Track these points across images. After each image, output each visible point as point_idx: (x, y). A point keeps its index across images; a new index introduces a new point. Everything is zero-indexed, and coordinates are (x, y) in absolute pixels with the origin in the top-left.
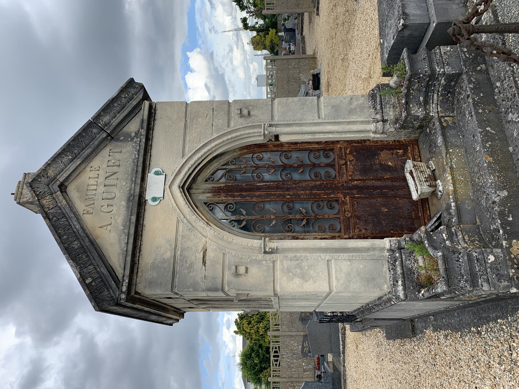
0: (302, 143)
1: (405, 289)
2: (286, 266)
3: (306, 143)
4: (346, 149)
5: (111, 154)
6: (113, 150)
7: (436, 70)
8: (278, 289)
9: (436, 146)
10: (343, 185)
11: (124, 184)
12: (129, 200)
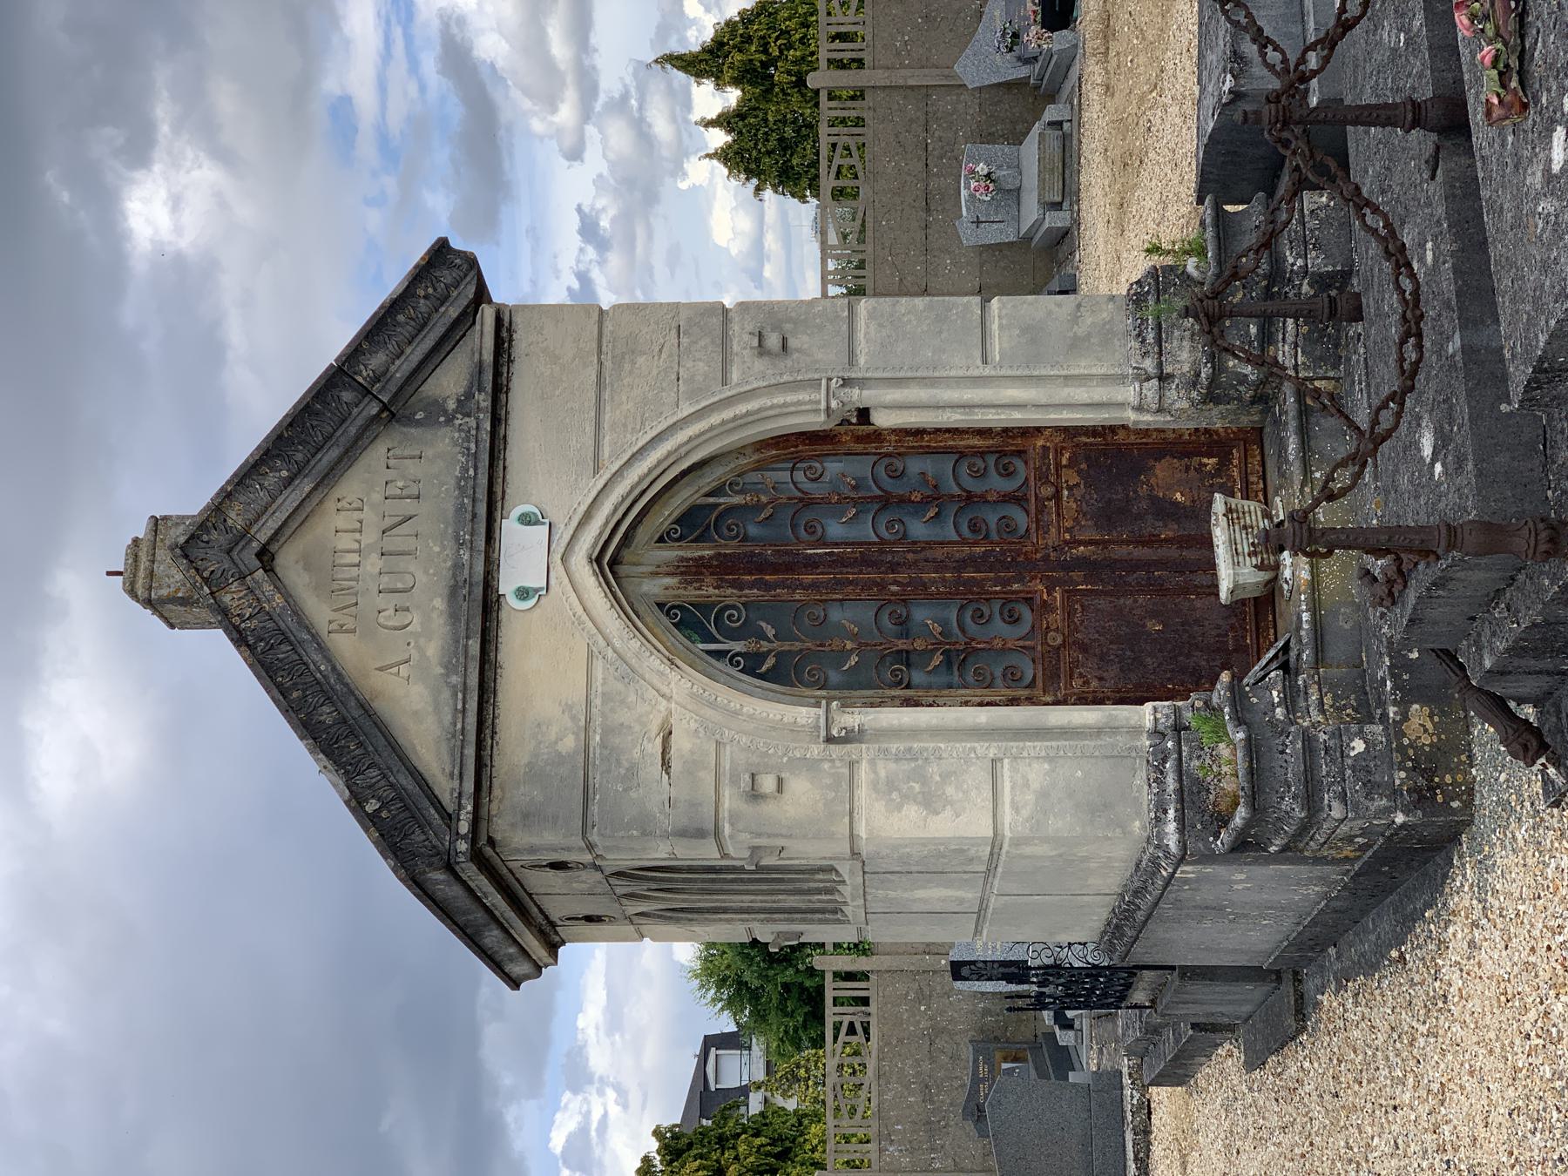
0: (937, 431)
1: (1181, 830)
2: (883, 774)
3: (948, 430)
4: (1059, 452)
5: (392, 462)
6: (398, 452)
7: (1285, 260)
8: (862, 831)
9: (1287, 461)
10: (1046, 558)
11: (437, 549)
12: (453, 592)
